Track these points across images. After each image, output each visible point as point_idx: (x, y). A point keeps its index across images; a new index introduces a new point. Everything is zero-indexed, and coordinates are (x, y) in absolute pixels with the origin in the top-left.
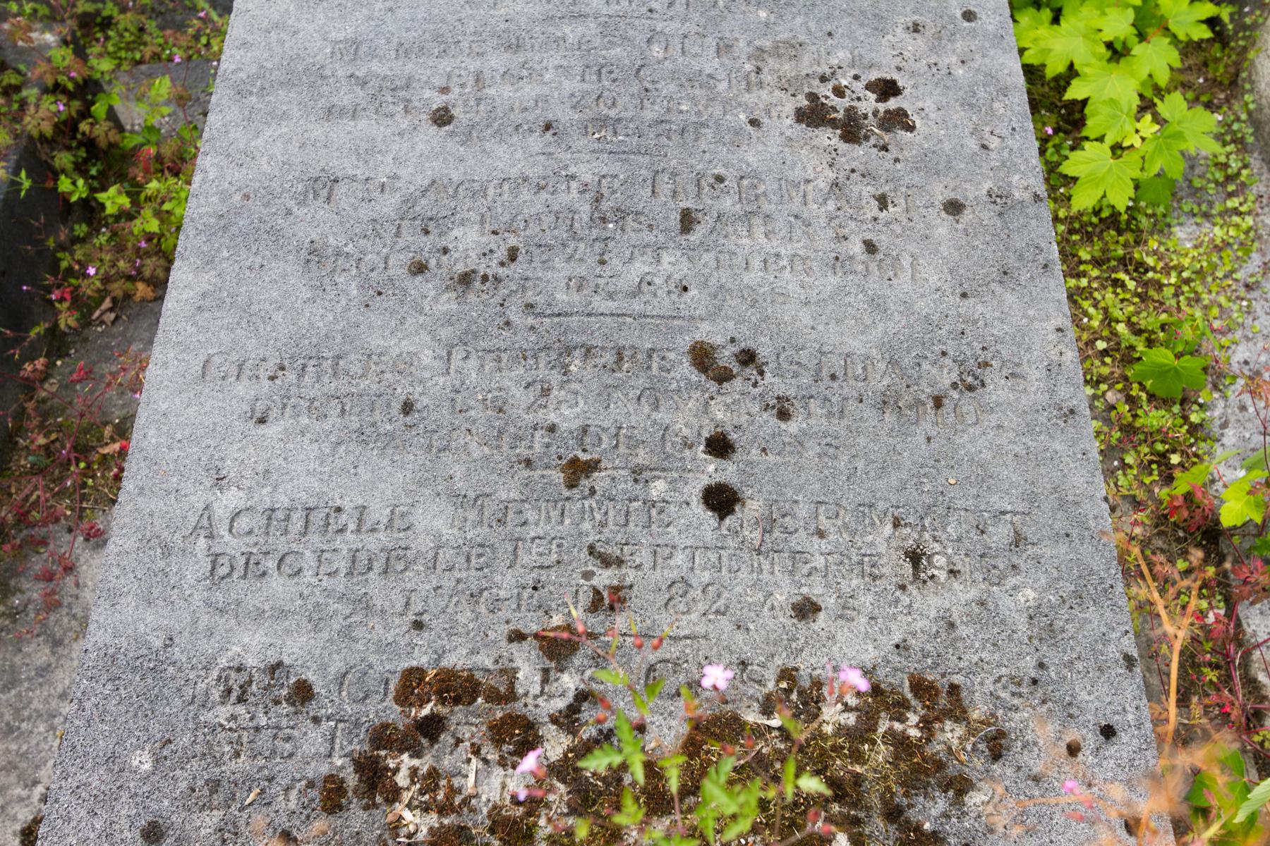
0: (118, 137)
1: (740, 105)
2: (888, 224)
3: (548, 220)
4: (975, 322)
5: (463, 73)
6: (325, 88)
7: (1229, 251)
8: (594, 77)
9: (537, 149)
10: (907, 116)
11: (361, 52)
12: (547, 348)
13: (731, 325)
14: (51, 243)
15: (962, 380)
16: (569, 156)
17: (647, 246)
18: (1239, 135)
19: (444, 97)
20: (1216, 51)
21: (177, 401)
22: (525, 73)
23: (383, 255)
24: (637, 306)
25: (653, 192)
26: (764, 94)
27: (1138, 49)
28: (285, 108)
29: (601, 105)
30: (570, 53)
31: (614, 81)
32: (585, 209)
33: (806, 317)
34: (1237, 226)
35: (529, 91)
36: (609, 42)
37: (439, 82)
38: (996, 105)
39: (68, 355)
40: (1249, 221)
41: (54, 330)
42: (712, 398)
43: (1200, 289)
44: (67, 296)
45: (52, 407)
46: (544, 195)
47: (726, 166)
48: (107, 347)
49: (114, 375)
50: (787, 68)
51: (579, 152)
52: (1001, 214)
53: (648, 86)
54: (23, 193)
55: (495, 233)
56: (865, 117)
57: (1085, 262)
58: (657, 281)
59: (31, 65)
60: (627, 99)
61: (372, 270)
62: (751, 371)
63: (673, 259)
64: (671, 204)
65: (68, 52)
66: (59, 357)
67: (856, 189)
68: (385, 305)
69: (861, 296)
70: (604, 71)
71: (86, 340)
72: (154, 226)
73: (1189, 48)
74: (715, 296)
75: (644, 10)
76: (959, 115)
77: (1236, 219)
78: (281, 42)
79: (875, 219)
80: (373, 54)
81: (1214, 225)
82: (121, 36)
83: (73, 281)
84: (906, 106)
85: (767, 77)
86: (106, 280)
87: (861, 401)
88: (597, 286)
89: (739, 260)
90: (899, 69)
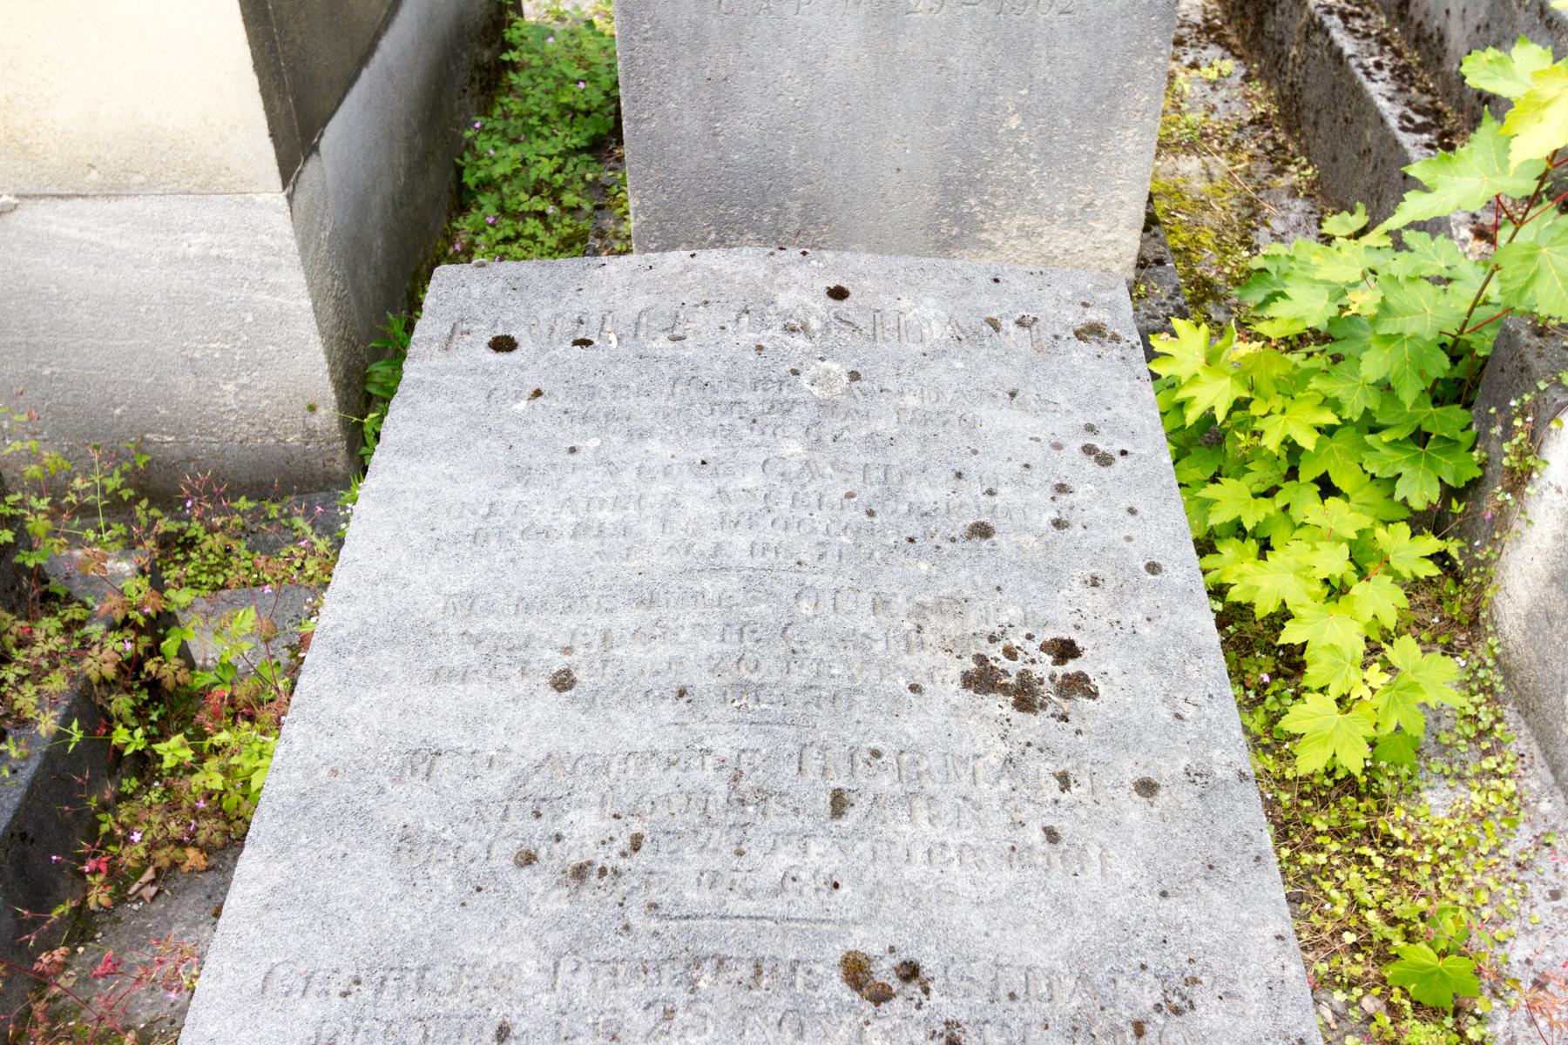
0: (187, 677)
1: (899, 668)
2: (1071, 807)
3: (678, 802)
4: (1179, 927)
5: (588, 631)
6: (434, 646)
7: (1492, 822)
8: (736, 637)
9: (668, 719)
10: (1088, 681)
11: (476, 607)
12: (672, 959)
13: (889, 930)
14: (93, 802)
15: (1166, 1001)
16: (704, 727)
17: (792, 833)
18: (1488, 684)
19: (567, 658)
20: (1449, 586)
21: (229, 1023)
22: (658, 631)
23: (486, 842)
24: (779, 907)
25: (800, 769)
26: (926, 655)
27: (1358, 589)
28: (386, 669)
29: (743, 668)
30: (709, 610)
31: (758, 641)
32: (721, 789)
33: (978, 921)
34: (1497, 790)
35: (662, 652)
36: (753, 597)
37: (562, 641)
38: (1189, 668)
39: (93, 939)
40: (1511, 785)
41: (81, 911)
42: (867, 1023)
43: (1461, 868)
44: (103, 867)
45: (64, 1007)
46: (675, 772)
47: (882, 738)
48: (142, 929)
49: (146, 966)
50: (952, 627)
51: (716, 722)
52: (1201, 796)
53: (796, 647)
54: (71, 747)
55: (616, 817)
56: (1041, 682)
57: (1321, 833)
58: (804, 876)
59: (101, 598)
60: (771, 662)
61: (472, 861)
62: (914, 989)
63: (822, 850)
64: (820, 784)
65: (143, 583)
66: (82, 943)
67: (1033, 766)
68: (484, 903)
69: (1042, 895)
70: (746, 630)
71: (118, 920)
72: (217, 782)
73: (1414, 587)
74: (871, 895)
75: (792, 562)
76: (1147, 680)
77: (1495, 783)
78: (389, 596)
79: (1056, 802)
80: (490, 609)
81: (1471, 789)
82: (204, 558)
83: (111, 848)
84: (1086, 669)
85: (928, 636)
86: (153, 846)
87: (1047, 1027)
88: (733, 881)
89: (899, 851)
90: (1077, 627)
